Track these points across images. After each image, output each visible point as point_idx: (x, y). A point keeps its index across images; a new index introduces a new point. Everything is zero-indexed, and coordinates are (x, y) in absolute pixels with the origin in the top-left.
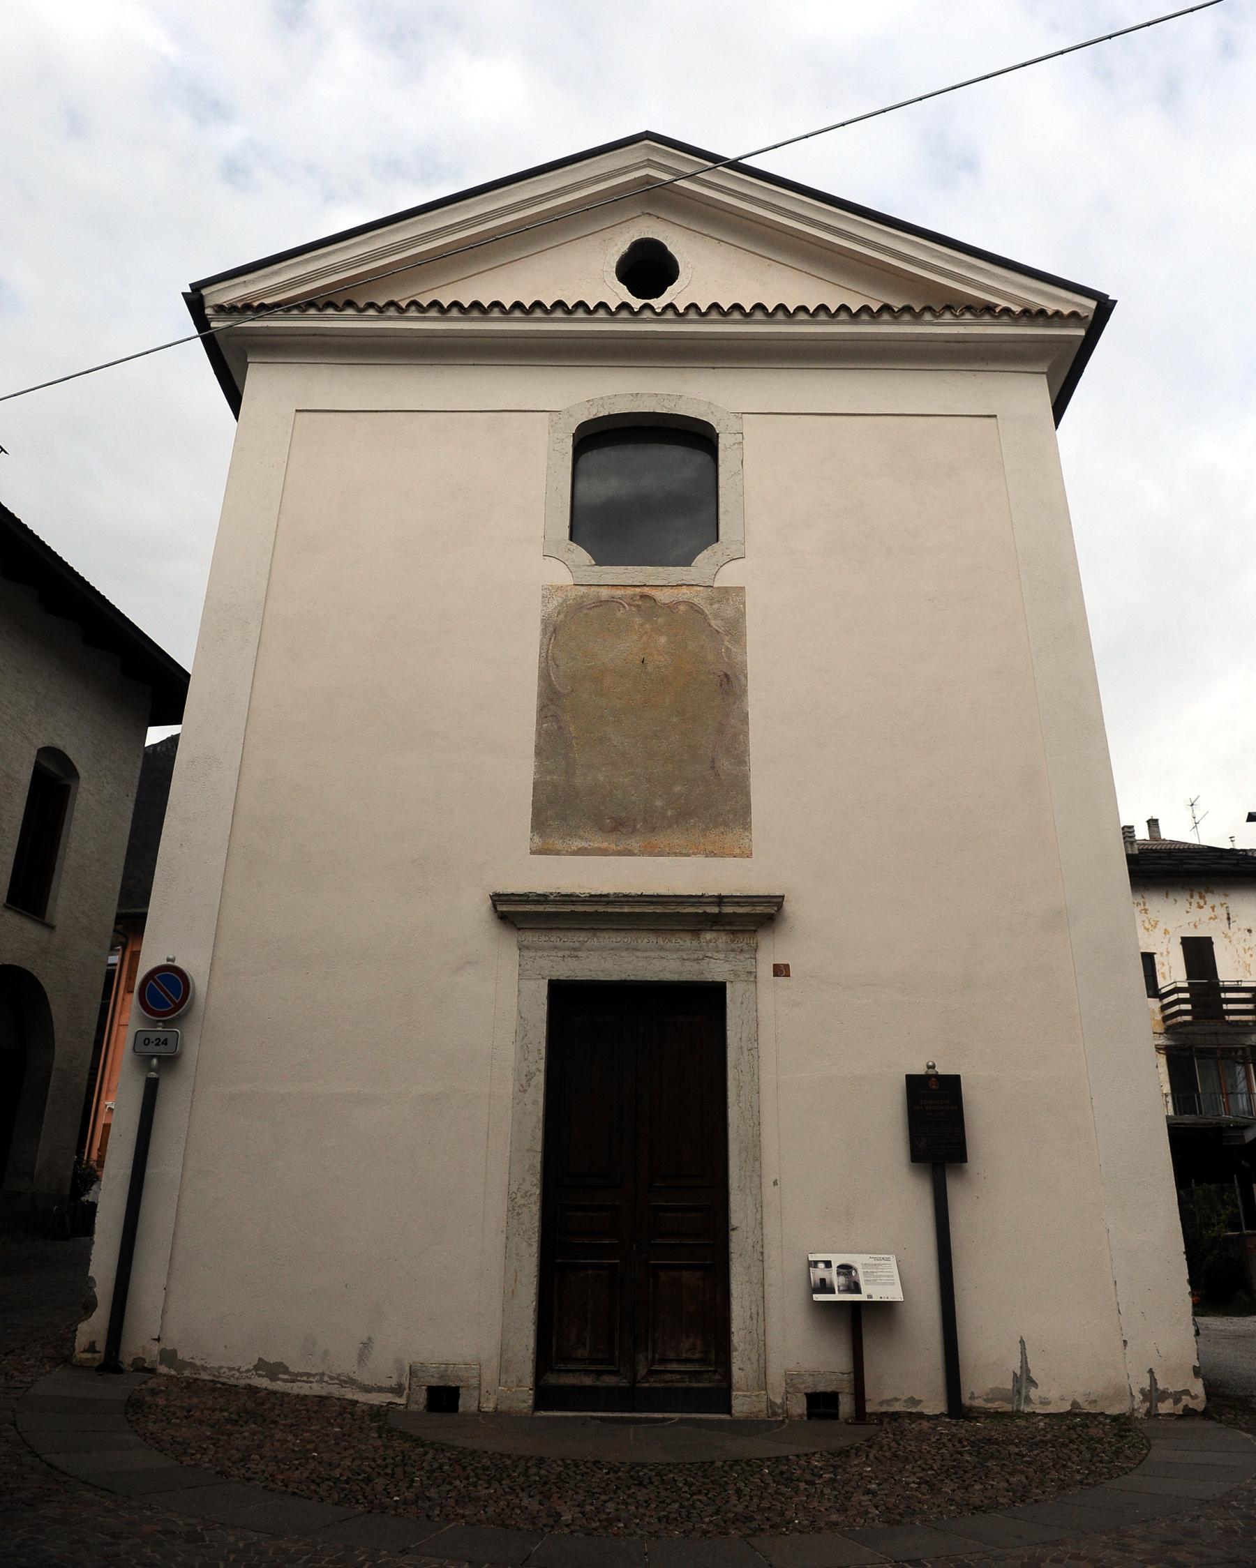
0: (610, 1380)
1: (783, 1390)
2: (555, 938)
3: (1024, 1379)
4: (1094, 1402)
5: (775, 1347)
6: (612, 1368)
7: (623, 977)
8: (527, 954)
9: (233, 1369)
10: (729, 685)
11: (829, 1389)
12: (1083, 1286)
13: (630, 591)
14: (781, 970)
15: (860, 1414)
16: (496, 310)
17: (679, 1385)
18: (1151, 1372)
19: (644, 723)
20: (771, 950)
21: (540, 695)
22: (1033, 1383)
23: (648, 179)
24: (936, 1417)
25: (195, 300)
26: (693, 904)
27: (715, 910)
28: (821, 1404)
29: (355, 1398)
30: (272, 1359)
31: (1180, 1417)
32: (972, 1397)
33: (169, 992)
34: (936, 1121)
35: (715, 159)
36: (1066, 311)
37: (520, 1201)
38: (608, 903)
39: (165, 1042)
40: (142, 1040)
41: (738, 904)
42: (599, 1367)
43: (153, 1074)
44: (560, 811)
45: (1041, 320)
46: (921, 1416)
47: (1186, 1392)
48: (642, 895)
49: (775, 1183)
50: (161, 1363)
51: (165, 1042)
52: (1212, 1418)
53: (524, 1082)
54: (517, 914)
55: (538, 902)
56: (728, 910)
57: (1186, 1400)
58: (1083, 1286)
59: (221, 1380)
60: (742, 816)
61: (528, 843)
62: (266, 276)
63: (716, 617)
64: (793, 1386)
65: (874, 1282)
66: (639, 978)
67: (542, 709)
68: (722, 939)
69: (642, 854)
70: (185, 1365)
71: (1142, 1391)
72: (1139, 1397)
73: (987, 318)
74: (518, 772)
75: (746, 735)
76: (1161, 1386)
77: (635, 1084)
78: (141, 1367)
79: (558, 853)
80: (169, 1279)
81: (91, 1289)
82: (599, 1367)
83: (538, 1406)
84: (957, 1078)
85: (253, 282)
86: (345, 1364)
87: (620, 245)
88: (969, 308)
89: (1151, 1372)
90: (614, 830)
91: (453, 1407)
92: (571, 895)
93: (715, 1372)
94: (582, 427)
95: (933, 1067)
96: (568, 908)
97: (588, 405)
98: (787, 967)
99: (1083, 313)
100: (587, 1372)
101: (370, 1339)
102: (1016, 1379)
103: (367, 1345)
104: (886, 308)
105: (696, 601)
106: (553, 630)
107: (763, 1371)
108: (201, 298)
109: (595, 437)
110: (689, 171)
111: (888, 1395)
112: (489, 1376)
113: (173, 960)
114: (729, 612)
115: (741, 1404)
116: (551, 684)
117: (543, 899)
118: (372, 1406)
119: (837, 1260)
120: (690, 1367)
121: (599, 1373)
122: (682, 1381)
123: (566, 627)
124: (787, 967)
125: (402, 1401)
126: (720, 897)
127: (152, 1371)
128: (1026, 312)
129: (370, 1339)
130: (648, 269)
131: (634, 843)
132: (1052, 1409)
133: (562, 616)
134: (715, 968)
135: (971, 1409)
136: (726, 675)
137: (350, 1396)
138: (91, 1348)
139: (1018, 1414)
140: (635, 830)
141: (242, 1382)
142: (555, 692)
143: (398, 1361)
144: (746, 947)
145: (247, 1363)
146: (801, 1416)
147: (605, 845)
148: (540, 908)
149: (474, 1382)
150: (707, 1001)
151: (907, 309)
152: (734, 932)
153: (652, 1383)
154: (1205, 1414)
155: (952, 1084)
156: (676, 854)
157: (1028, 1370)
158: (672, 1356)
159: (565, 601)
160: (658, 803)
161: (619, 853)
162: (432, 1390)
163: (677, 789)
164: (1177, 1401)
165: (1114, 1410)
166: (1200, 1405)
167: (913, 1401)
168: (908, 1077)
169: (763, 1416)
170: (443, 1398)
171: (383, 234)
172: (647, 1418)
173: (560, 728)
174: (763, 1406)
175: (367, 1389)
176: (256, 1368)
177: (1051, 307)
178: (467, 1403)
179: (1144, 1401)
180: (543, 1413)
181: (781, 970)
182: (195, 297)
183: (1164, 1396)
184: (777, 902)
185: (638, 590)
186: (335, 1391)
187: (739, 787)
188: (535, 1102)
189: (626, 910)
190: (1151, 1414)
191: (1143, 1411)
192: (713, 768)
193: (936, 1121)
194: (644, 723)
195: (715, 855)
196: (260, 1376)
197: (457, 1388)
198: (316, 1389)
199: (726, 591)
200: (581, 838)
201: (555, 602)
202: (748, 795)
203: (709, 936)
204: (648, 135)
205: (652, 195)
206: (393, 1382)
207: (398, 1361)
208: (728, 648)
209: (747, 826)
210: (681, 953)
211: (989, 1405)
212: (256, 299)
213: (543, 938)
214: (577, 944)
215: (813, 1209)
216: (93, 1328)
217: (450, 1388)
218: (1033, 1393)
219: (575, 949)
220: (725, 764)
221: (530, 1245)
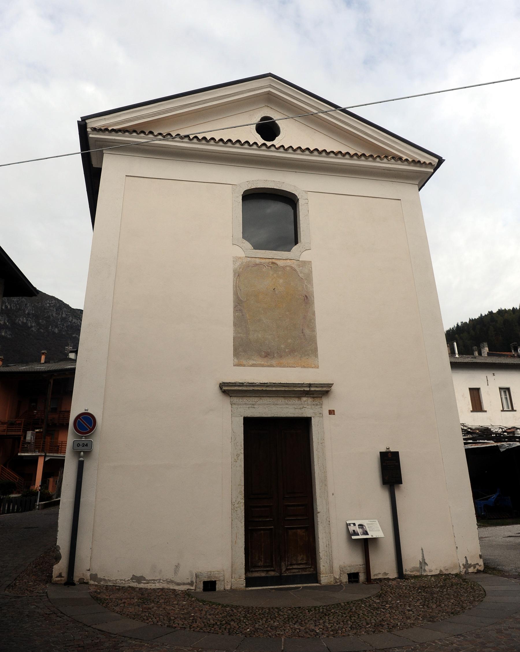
0: (272, 574)
1: (339, 573)
2: (245, 400)
3: (423, 563)
4: (447, 570)
5: (335, 558)
6: (272, 569)
7: (272, 416)
8: (234, 406)
9: (122, 580)
10: (307, 300)
11: (356, 572)
12: (443, 528)
13: (267, 261)
14: (332, 412)
15: (368, 579)
16: (212, 141)
17: (298, 573)
18: (466, 557)
19: (275, 315)
20: (327, 404)
21: (234, 302)
22: (426, 564)
23: (269, 93)
24: (393, 579)
25: (82, 126)
26: (300, 387)
27: (308, 389)
28: (353, 577)
29: (174, 588)
30: (138, 575)
31: (476, 573)
32: (406, 571)
33: (87, 423)
34: (390, 469)
35: (336, 107)
36: (427, 162)
37: (236, 505)
38: (267, 386)
39: (87, 445)
40: (76, 445)
41: (316, 387)
42: (267, 569)
43: (81, 459)
44: (244, 349)
45: (418, 164)
46: (388, 579)
47: (477, 564)
48: (280, 383)
49: (333, 494)
50: (91, 580)
51: (87, 445)
52: (486, 573)
53: (236, 458)
54: (229, 390)
55: (239, 386)
56: (312, 389)
57: (477, 567)
58: (443, 528)
59: (117, 585)
60: (315, 351)
61: (232, 362)
62: (114, 117)
63: (301, 272)
64: (343, 571)
65: (372, 530)
66: (279, 416)
67: (235, 307)
68: (310, 400)
69: (277, 366)
70: (101, 580)
71: (463, 565)
72: (462, 567)
73: (399, 162)
74: (226, 333)
75: (315, 320)
76: (469, 563)
77: (278, 458)
78: (83, 582)
79: (244, 366)
80: (92, 545)
81: (58, 550)
82: (267, 569)
83: (247, 586)
84: (398, 453)
85: (108, 119)
86: (170, 576)
87: (257, 119)
88: (393, 158)
89: (466, 557)
90: (266, 356)
91: (214, 589)
92: (253, 383)
93: (311, 568)
94: (245, 192)
95: (389, 449)
96: (251, 388)
97: (247, 183)
98: (334, 411)
99: (433, 164)
100: (263, 571)
101: (178, 564)
102: (421, 563)
103: (177, 566)
104: (363, 155)
105: (293, 266)
106: (238, 275)
107: (331, 567)
108: (86, 124)
109: (251, 196)
110: (325, 110)
111: (376, 572)
112: (228, 575)
113: (87, 410)
114: (306, 271)
115: (325, 579)
116: (238, 297)
117: (242, 384)
118: (182, 591)
119: (357, 523)
120: (302, 566)
121: (268, 571)
122: (299, 572)
123: (243, 273)
124: (334, 411)
125: (193, 588)
126: (310, 384)
127: (87, 583)
128: (413, 161)
129: (178, 564)
130: (268, 130)
131: (274, 362)
132: (433, 573)
133: (241, 269)
134: (306, 413)
135: (405, 575)
136: (306, 296)
137: (172, 588)
138: (60, 575)
139: (421, 576)
140: (274, 357)
141: (126, 585)
142: (241, 300)
143: (191, 572)
144: (318, 404)
145: (128, 577)
146: (346, 582)
147: (263, 363)
148: (240, 388)
149: (222, 578)
150: (305, 423)
151: (371, 156)
152: (313, 397)
153: (288, 574)
154: (484, 572)
155: (395, 455)
156: (290, 367)
157: (424, 560)
158: (295, 563)
159: (242, 263)
160: (283, 346)
161: (268, 366)
162: (205, 583)
163: (289, 341)
164: (474, 568)
165: (454, 572)
166: (482, 568)
167: (386, 574)
168: (380, 452)
169: (332, 583)
170: (210, 586)
171: (164, 104)
172: (310, 587)
173: (243, 315)
174: (332, 579)
175: (178, 584)
176: (132, 579)
177: (422, 160)
178: (219, 587)
179: (464, 568)
180: (250, 588)
181: (332, 412)
182: (83, 123)
183: (470, 566)
184: (330, 385)
185: (270, 260)
186: (165, 586)
187: (313, 340)
188: (240, 466)
189: (274, 389)
190: (467, 573)
191: (464, 572)
192: (303, 333)
193: (390, 469)
194: (275, 315)
195: (305, 367)
196: (134, 582)
197: (215, 581)
198: (158, 586)
199: (304, 262)
200: (253, 360)
201: (238, 264)
202: (316, 344)
203: (304, 399)
204: (270, 75)
205: (270, 99)
206: (189, 581)
207: (191, 572)
208: (306, 285)
209: (316, 356)
210: (294, 406)
211: (412, 573)
212: (110, 126)
213: (240, 400)
214: (254, 403)
215: (345, 503)
216: (60, 568)
217: (212, 581)
218: (427, 568)
219: (253, 405)
220: (307, 331)
221: (241, 523)
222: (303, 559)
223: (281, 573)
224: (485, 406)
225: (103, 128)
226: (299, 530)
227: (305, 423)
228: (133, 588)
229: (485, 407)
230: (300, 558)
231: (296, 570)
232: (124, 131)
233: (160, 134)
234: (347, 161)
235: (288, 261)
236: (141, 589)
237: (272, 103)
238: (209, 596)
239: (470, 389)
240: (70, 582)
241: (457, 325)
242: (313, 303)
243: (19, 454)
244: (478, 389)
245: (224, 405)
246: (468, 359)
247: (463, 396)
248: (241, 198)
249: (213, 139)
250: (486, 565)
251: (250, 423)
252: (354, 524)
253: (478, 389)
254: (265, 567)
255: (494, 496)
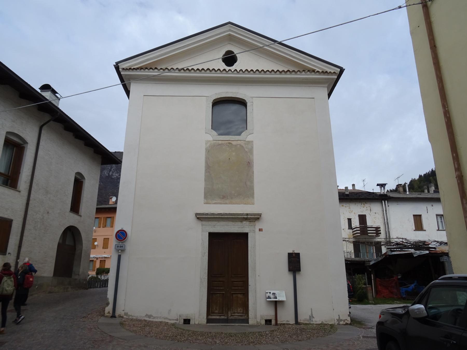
0: (223, 317)
2: (210, 223)
3: (312, 317)
5: (258, 310)
10: (249, 164)
14: (260, 230)
15: (276, 324)
20: (258, 225)
22: (313, 317)
23: (230, 35)
25: (117, 68)
27: (246, 217)
28: (268, 322)
30: (149, 314)
34: (294, 263)
35: (275, 41)
44: (210, 195)
45: (326, 74)
46: (289, 324)
47: (346, 320)
54: (201, 217)
55: (201, 215)
56: (249, 217)
60: (252, 195)
67: (206, 170)
69: (229, 204)
70: (130, 316)
72: (336, 321)
73: (313, 73)
76: (341, 318)
77: (228, 256)
78: (120, 316)
79: (210, 204)
83: (207, 323)
85: (131, 62)
88: (309, 71)
90: (223, 198)
96: (213, 216)
99: (336, 72)
102: (310, 317)
103: (170, 311)
106: (208, 151)
109: (217, 103)
110: (268, 44)
117: (207, 214)
119: (272, 292)
120: (240, 314)
121: (220, 316)
123: (212, 150)
125: (178, 322)
128: (323, 72)
130: (230, 59)
131: (227, 201)
138: (109, 313)
141: (143, 319)
148: (206, 216)
149: (193, 318)
150: (245, 236)
154: (350, 324)
155: (298, 255)
160: (233, 192)
163: (237, 189)
166: (349, 322)
167: (288, 321)
169: (256, 324)
170: (187, 321)
175: (170, 320)
176: (146, 316)
177: (329, 71)
181: (260, 230)
182: (117, 66)
183: (341, 320)
184: (260, 215)
187: (252, 188)
189: (226, 217)
193: (294, 263)
199: (249, 142)
201: (208, 145)
202: (254, 190)
203: (244, 222)
205: (231, 39)
206: (176, 318)
212: (132, 66)
216: (109, 309)
218: (313, 320)
222: (241, 310)
223: (228, 317)
224: (425, 227)
225: (128, 68)
226: (239, 295)
227: (245, 236)
228: (145, 321)
229: (425, 228)
230: (239, 310)
231: (236, 316)
232: (141, 68)
233: (161, 69)
234: (278, 76)
235: (239, 142)
236: (150, 321)
237: (231, 41)
238: (186, 327)
239: (414, 216)
240: (113, 316)
241: (432, 170)
242: (253, 166)
243: (372, 275)
244: (420, 216)
245: (198, 226)
246: (415, 195)
247: (408, 220)
248: (211, 104)
249: (193, 69)
250: (352, 320)
251: (212, 236)
252: (270, 293)
253: (420, 216)
254: (219, 313)
255: (413, 286)
